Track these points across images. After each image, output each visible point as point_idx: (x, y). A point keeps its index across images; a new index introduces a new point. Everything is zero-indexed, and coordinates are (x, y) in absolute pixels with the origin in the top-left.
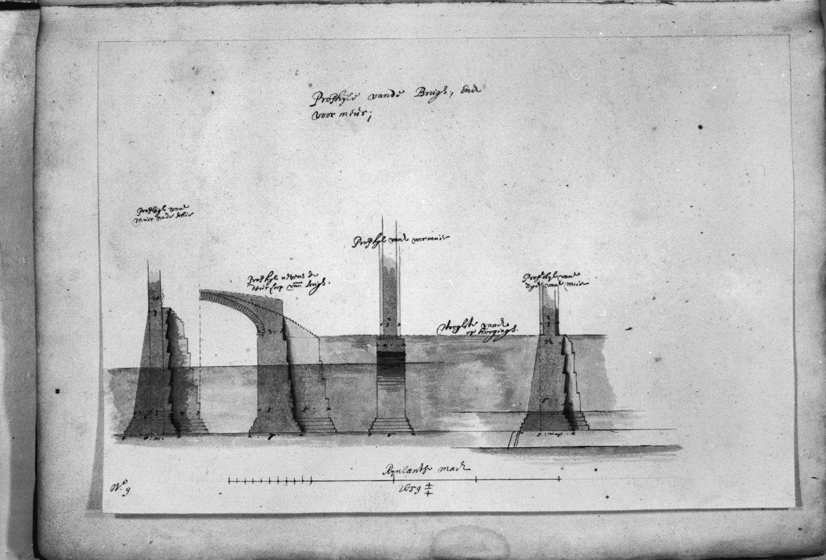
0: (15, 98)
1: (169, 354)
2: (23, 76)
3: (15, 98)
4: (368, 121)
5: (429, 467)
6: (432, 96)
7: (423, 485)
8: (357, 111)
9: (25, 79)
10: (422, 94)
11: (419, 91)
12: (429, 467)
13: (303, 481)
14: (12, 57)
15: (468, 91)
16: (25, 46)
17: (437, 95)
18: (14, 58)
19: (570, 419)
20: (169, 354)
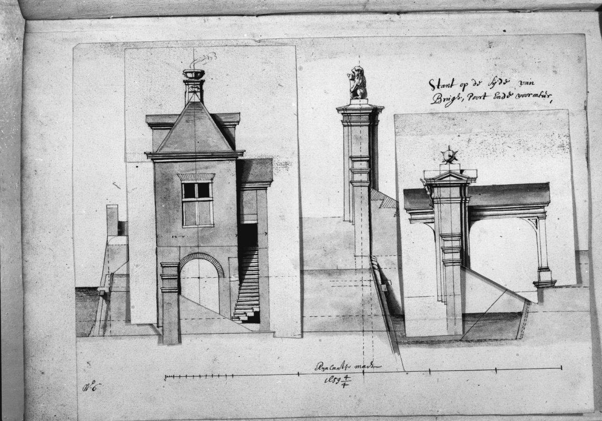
0: (9, 56)
1: (385, 286)
2: (16, 38)
3: (9, 56)
4: (550, 103)
5: (349, 366)
6: (448, 101)
7: (342, 377)
8: (544, 94)
9: (17, 41)
10: (440, 100)
11: (436, 96)
12: (349, 366)
13: (193, 376)
14: (6, 23)
15: (499, 97)
16: (17, 15)
17: (453, 100)
18: (8, 24)
19: (255, 319)
20: (385, 286)
